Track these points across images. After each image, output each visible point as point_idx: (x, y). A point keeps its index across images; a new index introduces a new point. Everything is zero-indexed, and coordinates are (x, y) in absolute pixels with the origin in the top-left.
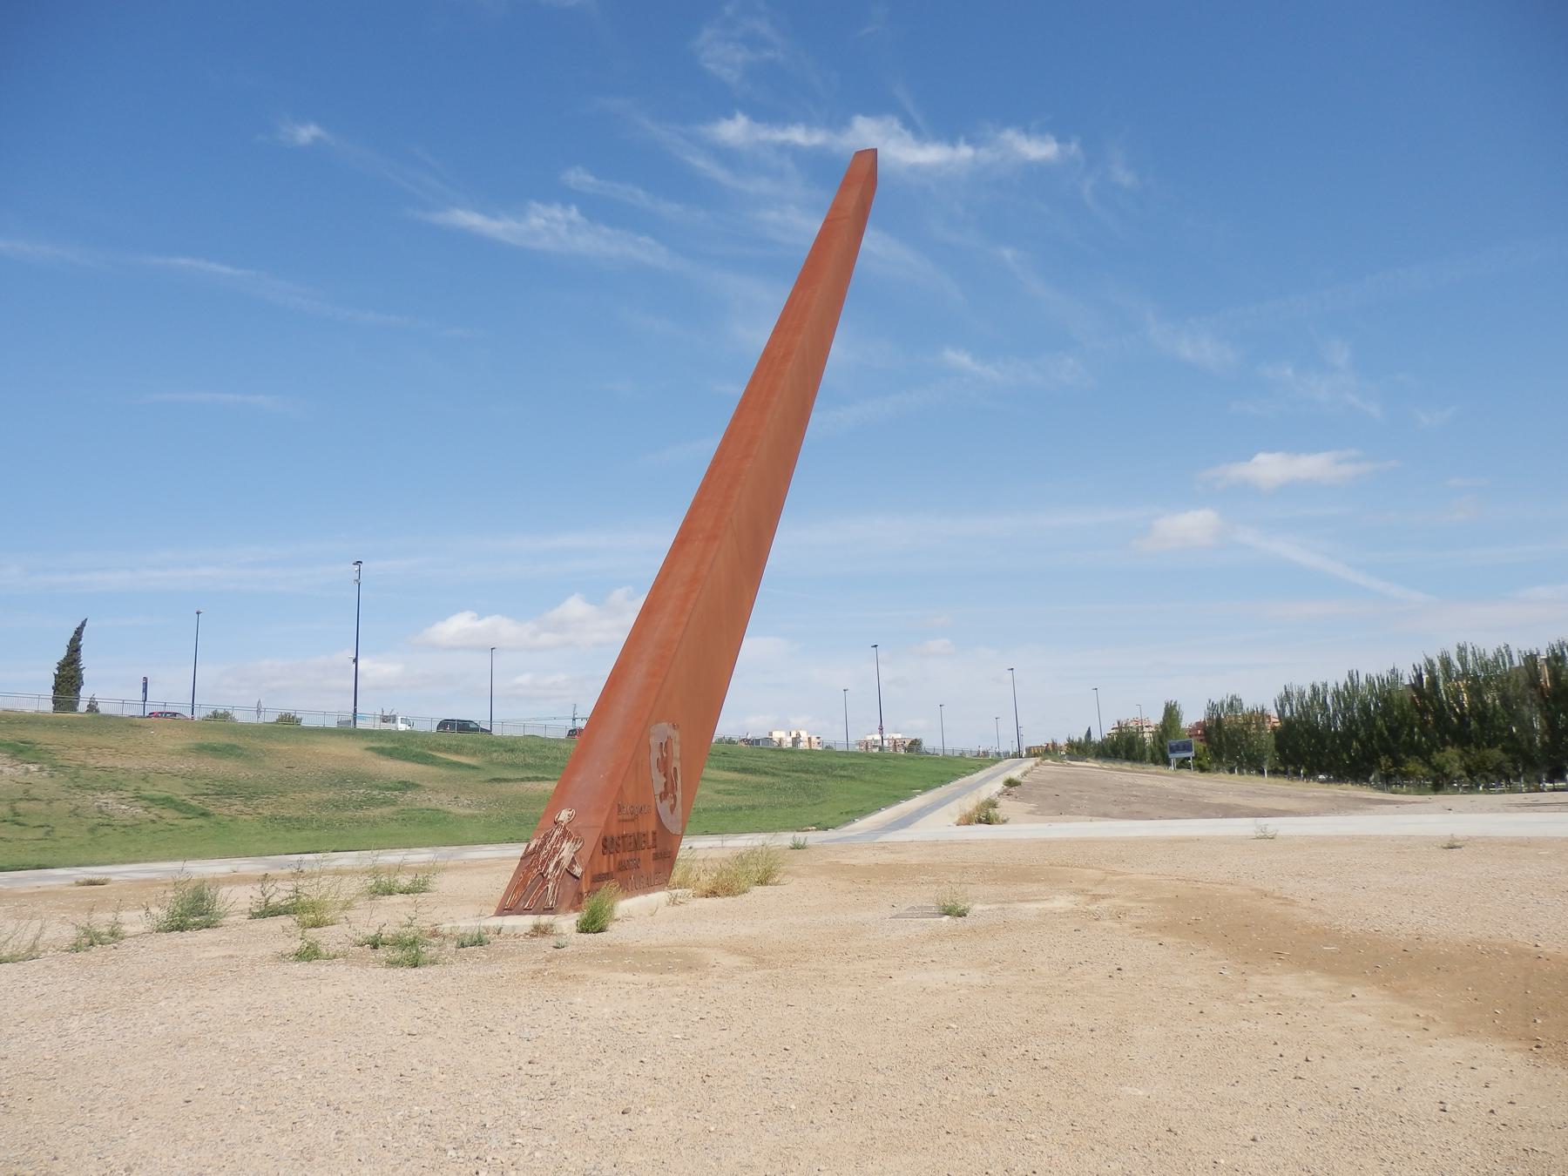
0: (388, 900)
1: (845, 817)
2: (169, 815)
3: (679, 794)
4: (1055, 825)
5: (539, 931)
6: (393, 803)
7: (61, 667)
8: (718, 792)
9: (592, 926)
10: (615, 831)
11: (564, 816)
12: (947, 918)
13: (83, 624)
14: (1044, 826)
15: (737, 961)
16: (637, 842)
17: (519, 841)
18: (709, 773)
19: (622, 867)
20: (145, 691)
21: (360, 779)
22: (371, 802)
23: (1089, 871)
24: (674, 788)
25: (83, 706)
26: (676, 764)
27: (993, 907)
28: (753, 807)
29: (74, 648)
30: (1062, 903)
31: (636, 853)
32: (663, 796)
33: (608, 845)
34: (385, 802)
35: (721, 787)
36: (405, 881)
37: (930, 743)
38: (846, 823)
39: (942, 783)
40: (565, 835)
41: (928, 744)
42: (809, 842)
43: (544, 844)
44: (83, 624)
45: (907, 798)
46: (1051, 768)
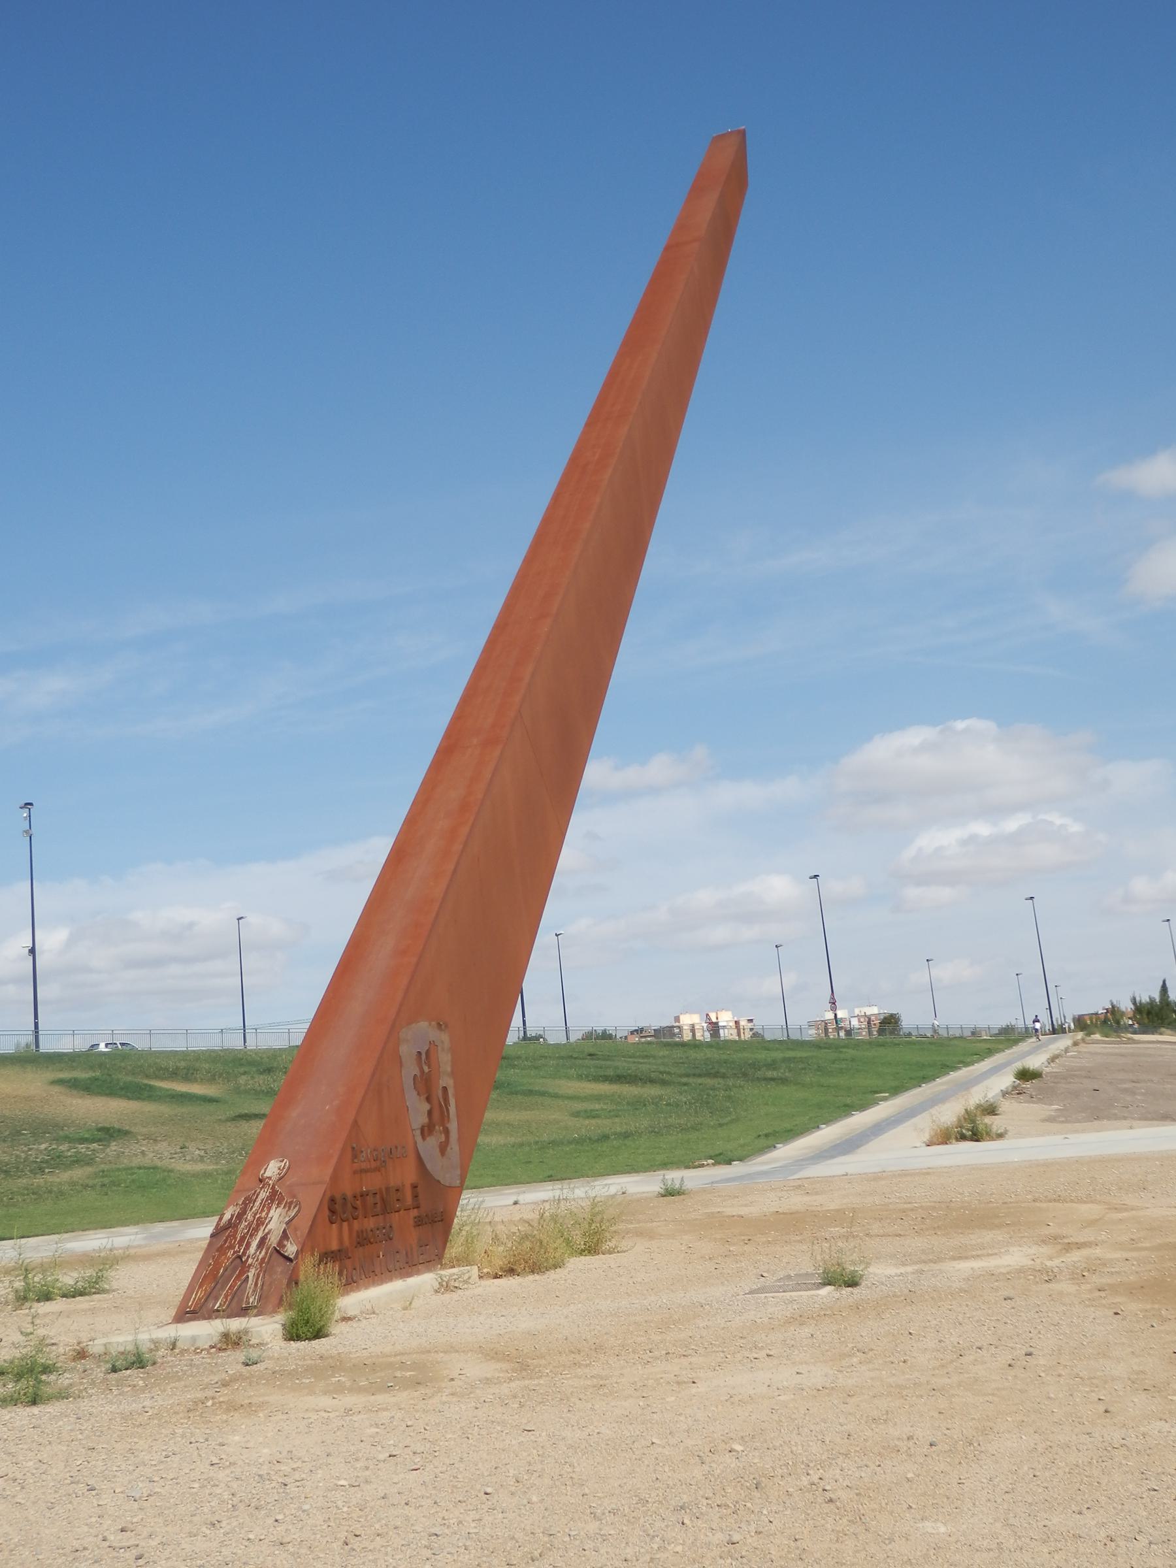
0: (44, 1308)
1: (763, 1142)
3: (453, 1126)
4: (1074, 1138)
5: (230, 1341)
6: (89, 1161)
8: (576, 1114)
9: (308, 1327)
10: (347, 1187)
11: (272, 1169)
12: (829, 1288)
14: (1058, 1139)
15: (491, 1369)
16: (385, 1202)
17: (205, 1214)
19: (363, 1240)
21: (41, 1128)
22: (57, 1161)
23: (1084, 1208)
24: (444, 1117)
26: (447, 1081)
27: (909, 1269)
28: (626, 1135)
30: (1016, 1257)
31: (384, 1215)
32: (427, 1131)
33: (336, 1208)
34: (78, 1161)
35: (578, 1106)
36: (68, 1279)
37: (914, 1018)
38: (762, 1150)
39: (925, 1079)
41: (908, 1022)
42: (688, 1185)
43: (243, 1213)
45: (862, 1107)
46: (1100, 1046)
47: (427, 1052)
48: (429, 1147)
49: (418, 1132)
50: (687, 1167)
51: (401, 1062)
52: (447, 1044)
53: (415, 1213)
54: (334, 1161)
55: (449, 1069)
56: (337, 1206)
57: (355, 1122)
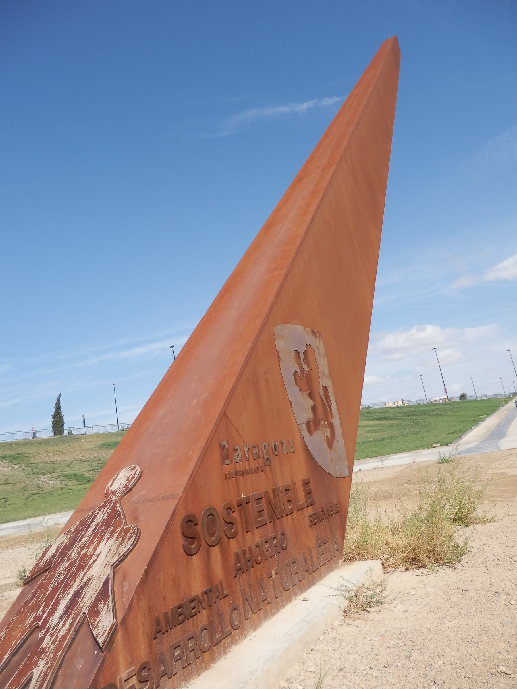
1: (455, 435)
2: (72, 484)
3: (336, 421)
5: (360, 604)
7: (54, 417)
8: (369, 432)
13: (60, 396)
18: (361, 423)
20: (84, 422)
24: (328, 413)
25: (66, 433)
26: (325, 381)
28: (392, 438)
29: (58, 408)
32: (312, 425)
35: (369, 429)
37: (470, 394)
40: (112, 521)
41: (468, 395)
44: (60, 396)
47: (305, 353)
48: (316, 441)
49: (304, 427)
50: (428, 448)
51: (279, 356)
52: (322, 350)
53: (310, 511)
54: (191, 466)
55: (327, 372)
56: (199, 528)
57: (224, 414)
